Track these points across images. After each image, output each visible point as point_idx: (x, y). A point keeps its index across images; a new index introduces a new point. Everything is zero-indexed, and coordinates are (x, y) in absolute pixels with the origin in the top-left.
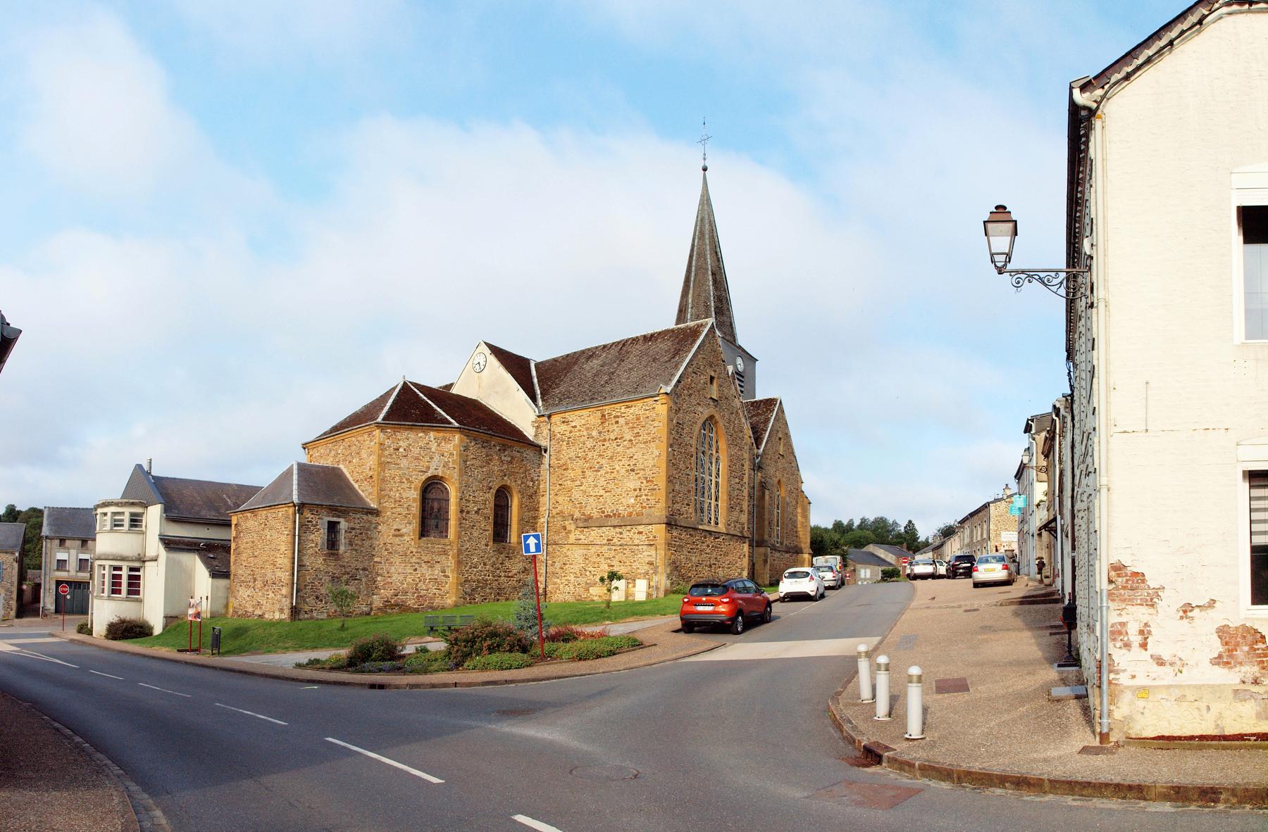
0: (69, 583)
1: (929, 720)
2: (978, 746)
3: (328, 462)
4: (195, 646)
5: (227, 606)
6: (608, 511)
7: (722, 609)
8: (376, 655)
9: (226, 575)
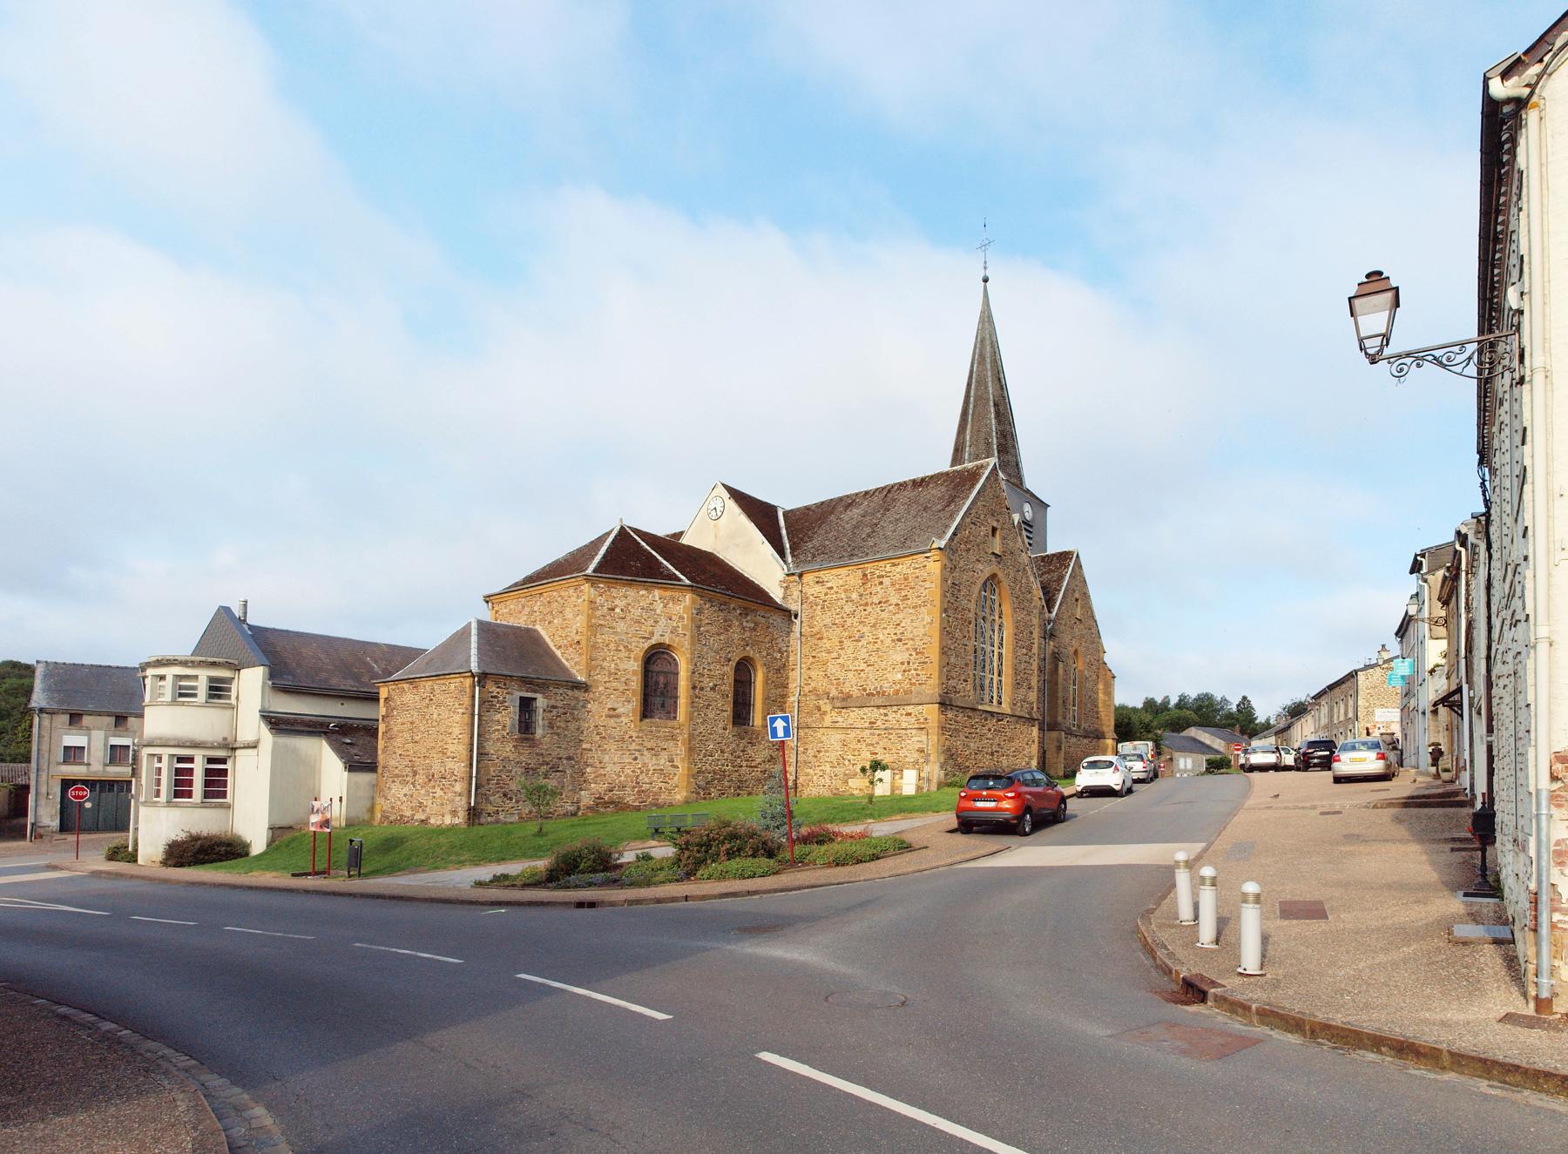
0: (90, 783)
1: (1271, 952)
2: (1341, 992)
3: (521, 621)
4: (320, 866)
5: (372, 810)
6: (871, 688)
7: (1006, 805)
8: (584, 866)
9: (371, 767)
